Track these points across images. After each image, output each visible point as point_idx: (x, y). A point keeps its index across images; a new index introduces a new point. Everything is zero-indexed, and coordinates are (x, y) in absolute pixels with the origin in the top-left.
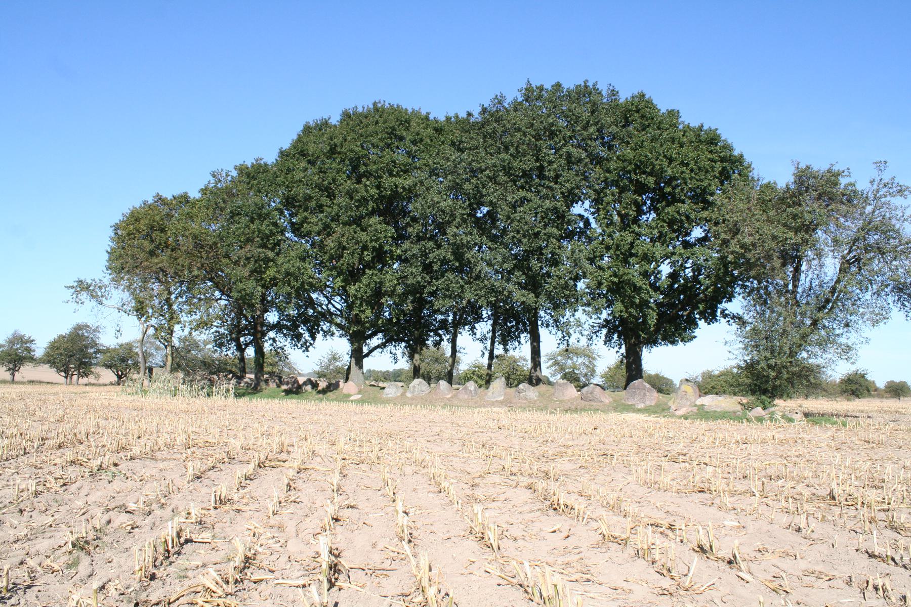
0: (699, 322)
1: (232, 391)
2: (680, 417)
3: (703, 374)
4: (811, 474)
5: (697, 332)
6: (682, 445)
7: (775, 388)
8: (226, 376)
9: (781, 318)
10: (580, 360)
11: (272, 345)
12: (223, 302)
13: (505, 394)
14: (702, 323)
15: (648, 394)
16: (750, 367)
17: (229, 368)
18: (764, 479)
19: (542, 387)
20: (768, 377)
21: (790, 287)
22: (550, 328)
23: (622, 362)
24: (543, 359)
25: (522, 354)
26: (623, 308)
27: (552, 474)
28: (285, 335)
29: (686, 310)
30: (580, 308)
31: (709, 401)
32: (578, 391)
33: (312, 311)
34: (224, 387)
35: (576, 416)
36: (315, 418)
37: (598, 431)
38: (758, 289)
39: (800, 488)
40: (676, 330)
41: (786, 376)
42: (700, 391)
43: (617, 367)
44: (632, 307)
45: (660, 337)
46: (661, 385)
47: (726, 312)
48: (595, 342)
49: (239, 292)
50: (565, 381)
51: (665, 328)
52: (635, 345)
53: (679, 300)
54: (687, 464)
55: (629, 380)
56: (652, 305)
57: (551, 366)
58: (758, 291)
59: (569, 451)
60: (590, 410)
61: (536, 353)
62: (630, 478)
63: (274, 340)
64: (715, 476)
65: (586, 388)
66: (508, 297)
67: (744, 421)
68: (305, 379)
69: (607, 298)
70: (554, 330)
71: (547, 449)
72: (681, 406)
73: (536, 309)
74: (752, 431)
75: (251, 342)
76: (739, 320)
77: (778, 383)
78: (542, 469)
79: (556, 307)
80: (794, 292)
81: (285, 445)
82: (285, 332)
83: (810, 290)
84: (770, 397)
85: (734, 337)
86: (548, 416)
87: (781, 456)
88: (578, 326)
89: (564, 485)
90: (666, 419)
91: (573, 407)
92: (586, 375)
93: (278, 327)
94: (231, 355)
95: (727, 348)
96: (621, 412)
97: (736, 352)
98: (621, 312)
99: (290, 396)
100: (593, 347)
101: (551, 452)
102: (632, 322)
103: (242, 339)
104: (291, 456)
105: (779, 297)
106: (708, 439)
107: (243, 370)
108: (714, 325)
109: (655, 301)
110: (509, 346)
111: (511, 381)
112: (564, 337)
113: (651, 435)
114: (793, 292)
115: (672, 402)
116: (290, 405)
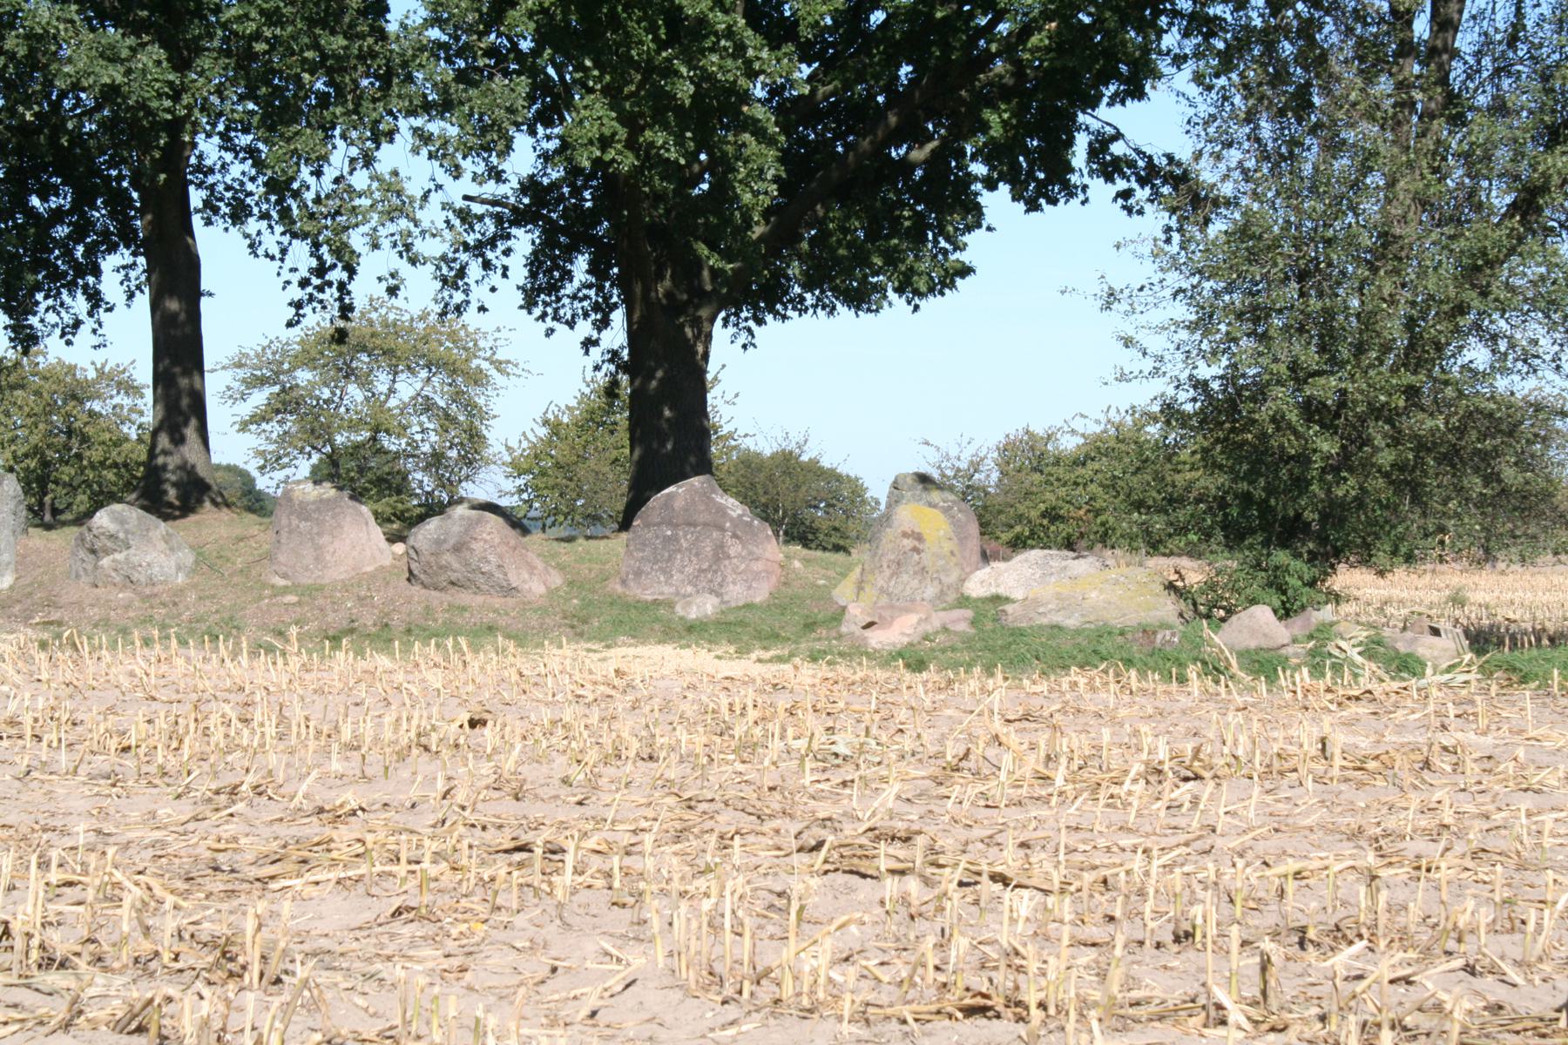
0: (986, 199)
2: (887, 659)
3: (1008, 451)
4: (1485, 916)
5: (976, 247)
6: (894, 788)
7: (1334, 513)
9: (1375, 179)
10: (407, 388)
13: (22, 563)
14: (998, 203)
15: (735, 548)
16: (1223, 415)
18: (1267, 945)
19: (211, 524)
20: (1303, 459)
21: (1421, 27)
22: (253, 225)
23: (611, 390)
24: (216, 383)
25: (112, 357)
26: (612, 125)
27: (252, 956)
29: (922, 138)
30: (404, 124)
31: (1029, 580)
32: (393, 538)
35: (383, 661)
37: (488, 734)
38: (1268, 37)
39: (1434, 981)
40: (873, 235)
41: (1386, 458)
42: (985, 527)
43: (591, 420)
44: (659, 120)
45: (795, 269)
46: (805, 507)
47: (1118, 149)
48: (479, 293)
50: (328, 490)
51: (821, 223)
52: (674, 308)
53: (890, 87)
54: (912, 885)
55: (648, 479)
56: (759, 112)
57: (258, 418)
58: (1270, 48)
59: (344, 834)
60: (452, 630)
61: (178, 347)
62: (636, 960)
64: (1042, 936)
65: (433, 524)
66: (32, 63)
67: (1192, 672)
69: (534, 72)
70: (271, 241)
71: (231, 829)
72: (899, 606)
73: (175, 127)
74: (1228, 719)
76: (1172, 183)
77: (1347, 488)
78: (207, 929)
79: (278, 116)
80: (1439, 52)
83: (1512, 41)
84: (1313, 557)
85: (1148, 271)
86: (246, 670)
87: (1356, 834)
88: (391, 215)
89: (314, 1006)
90: (822, 670)
91: (368, 620)
92: (436, 460)
95: (1116, 321)
96: (607, 638)
97: (1157, 343)
98: (605, 142)
100: (471, 317)
101: (251, 846)
102: (658, 197)
105: (1369, 77)
106: (1017, 759)
108: (1058, 215)
109: (775, 91)
110: (43, 317)
111: (55, 494)
112: (321, 271)
113: (748, 749)
114: (1433, 52)
115: (851, 588)
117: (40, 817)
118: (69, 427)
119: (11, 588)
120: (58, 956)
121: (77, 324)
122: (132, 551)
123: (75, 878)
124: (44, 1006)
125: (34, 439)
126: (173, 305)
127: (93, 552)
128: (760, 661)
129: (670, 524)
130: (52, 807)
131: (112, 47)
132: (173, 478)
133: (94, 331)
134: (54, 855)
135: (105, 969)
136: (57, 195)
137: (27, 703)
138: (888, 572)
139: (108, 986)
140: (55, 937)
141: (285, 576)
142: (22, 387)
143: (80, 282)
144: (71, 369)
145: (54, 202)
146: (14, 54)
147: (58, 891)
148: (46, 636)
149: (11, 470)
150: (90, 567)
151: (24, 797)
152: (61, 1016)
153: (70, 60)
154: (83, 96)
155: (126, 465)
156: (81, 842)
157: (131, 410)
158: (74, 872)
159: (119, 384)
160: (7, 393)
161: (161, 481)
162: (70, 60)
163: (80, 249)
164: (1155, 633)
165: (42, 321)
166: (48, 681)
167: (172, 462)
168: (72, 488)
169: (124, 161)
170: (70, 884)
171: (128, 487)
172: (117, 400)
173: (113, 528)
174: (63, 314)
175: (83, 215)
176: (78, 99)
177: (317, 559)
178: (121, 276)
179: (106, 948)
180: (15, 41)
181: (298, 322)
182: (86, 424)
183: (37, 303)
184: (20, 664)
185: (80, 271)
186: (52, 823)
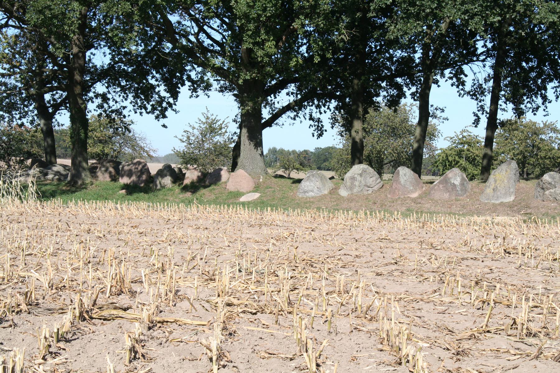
1: (32, 189)
8: (21, 162)
11: (100, 106)
12: (11, 32)
13: (517, 192)
17: (26, 148)
28: (123, 89)
33: (169, 45)
34: (17, 181)
36: (179, 234)
49: (41, 12)
63: (104, 97)
68: (160, 166)
75: (63, 103)
81: (127, 281)
82: (123, 83)
93: (110, 74)
94: (28, 125)
99: (135, 195)
103: (47, 97)
104: (138, 300)
107: (52, 152)
111: (528, 168)
116: (135, 212)
117: (525, 282)
118: (533, 144)
119: (513, 201)
120: (533, 332)
121: (538, 108)
122: (557, 189)
123: (538, 305)
124: (529, 350)
125: (521, 148)
127: (543, 189)
130: (529, 279)
131: (554, 8)
133: (544, 110)
134: (531, 296)
135: (550, 338)
136: (532, 62)
137: (519, 242)
139: (551, 345)
140: (532, 325)
142: (517, 130)
143: (539, 93)
144: (535, 123)
145: (530, 64)
146: (519, 11)
147: (532, 309)
148: (526, 218)
149: (513, 159)
150: (541, 194)
151: (519, 275)
152: (535, 354)
153: (538, 13)
154: (542, 26)
155: (553, 158)
156: (540, 292)
157: (556, 138)
158: (538, 303)
159: (551, 129)
160: (512, 132)
162: (538, 13)
163: (540, 81)
165: (526, 106)
166: (527, 234)
168: (534, 166)
169: (556, 49)
170: (536, 307)
171: (554, 166)
172: (551, 135)
173: (550, 180)
174: (533, 104)
175: (541, 69)
176: (541, 27)
178: (554, 90)
179: (550, 330)
180: (520, 7)
182: (539, 143)
183: (524, 100)
184: (517, 228)
185: (540, 89)
186: (529, 285)
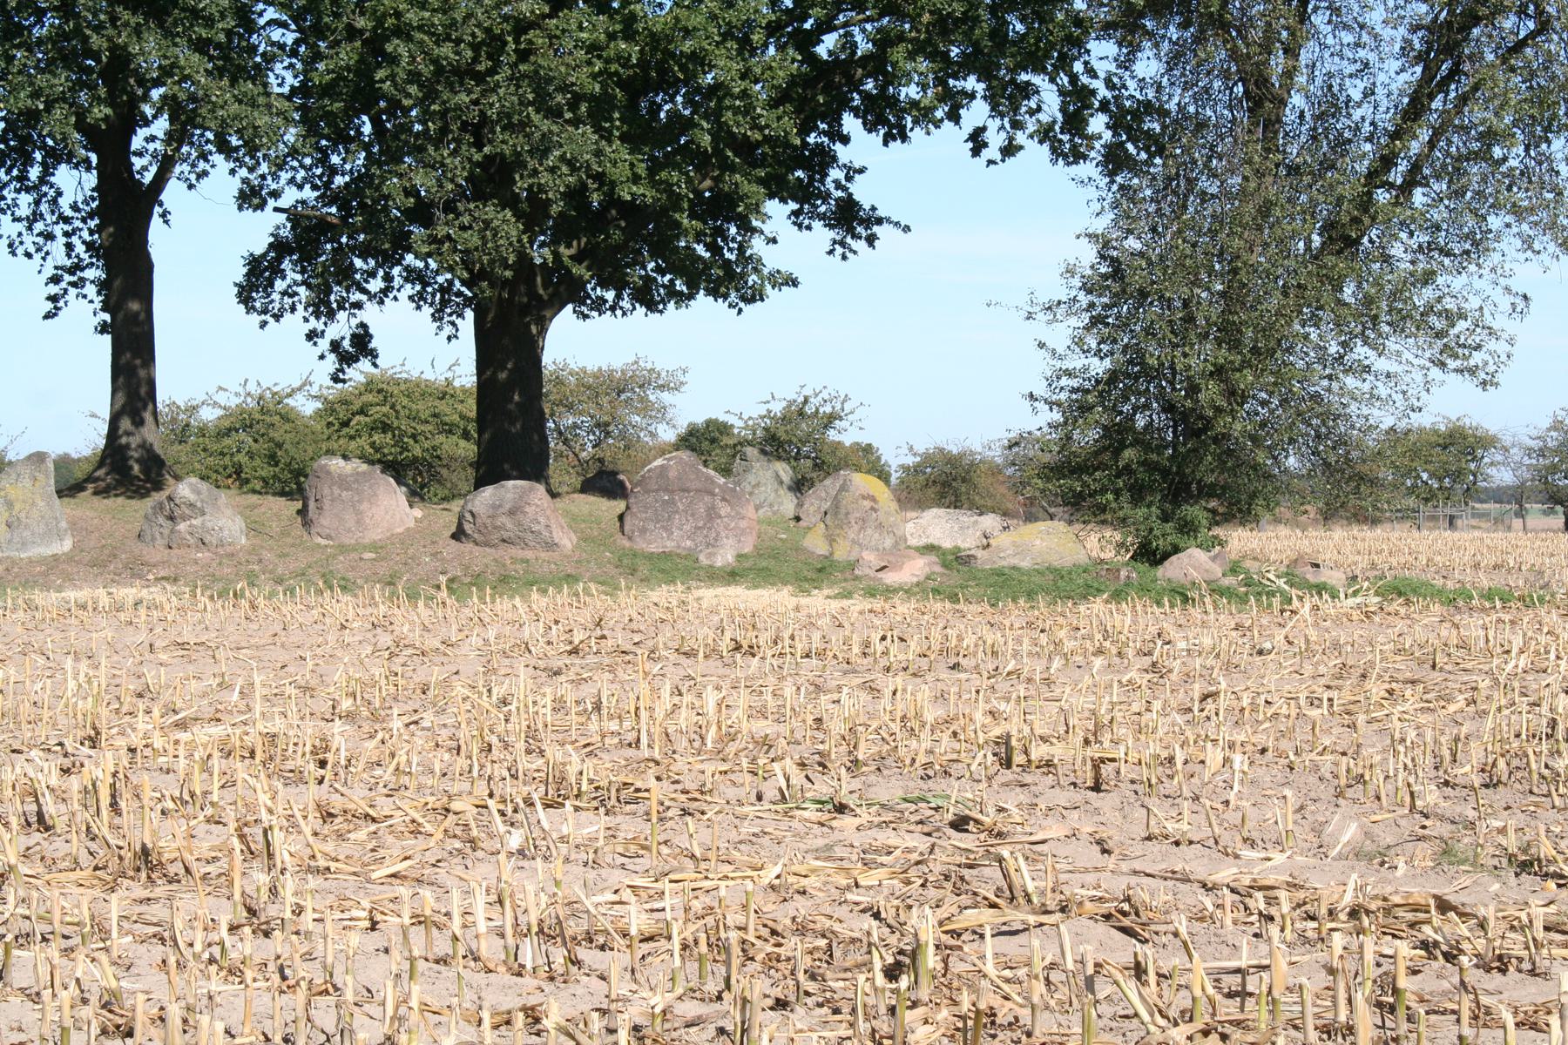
15: (725, 510)
122: (207, 517)
126: (135, 306)
127: (171, 518)
128: (828, 597)
129: (666, 490)
132: (136, 455)
138: (856, 527)
141: (328, 537)
150: (166, 532)
161: (126, 459)
164: (1118, 570)
167: (134, 441)
173: (192, 497)
177: (358, 522)
181: (55, 315)
